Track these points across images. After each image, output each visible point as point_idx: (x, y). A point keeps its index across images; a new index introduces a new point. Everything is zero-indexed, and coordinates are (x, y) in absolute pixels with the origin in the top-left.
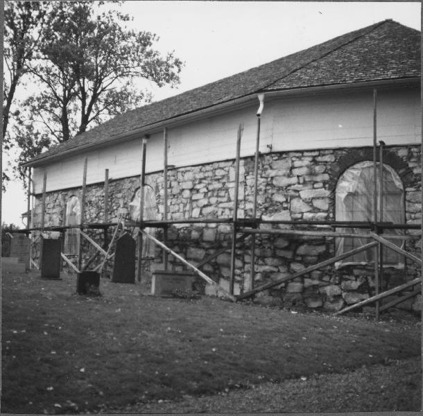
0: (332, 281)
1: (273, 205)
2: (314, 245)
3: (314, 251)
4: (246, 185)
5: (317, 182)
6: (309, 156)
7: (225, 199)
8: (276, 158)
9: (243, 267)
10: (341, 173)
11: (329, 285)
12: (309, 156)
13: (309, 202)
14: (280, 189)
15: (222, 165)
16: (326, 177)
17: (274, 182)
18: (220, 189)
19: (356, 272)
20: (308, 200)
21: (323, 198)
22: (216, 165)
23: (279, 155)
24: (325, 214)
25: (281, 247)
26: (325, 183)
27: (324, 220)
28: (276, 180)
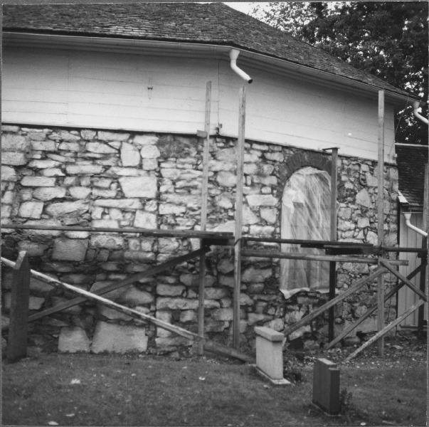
0: (276, 314)
1: (217, 212)
2: (262, 269)
3: (260, 277)
4: (160, 176)
5: (264, 186)
6: (258, 150)
7: (113, 194)
8: (222, 145)
9: (154, 303)
10: (288, 177)
11: (273, 319)
12: (258, 150)
13: (257, 212)
14: (225, 189)
15: (101, 136)
16: (274, 180)
17: (219, 179)
18: (99, 176)
19: (300, 300)
20: (255, 209)
21: (270, 207)
22: (91, 135)
23: (224, 141)
24: (271, 229)
25: (225, 272)
26: (273, 188)
27: (270, 236)
28: (222, 177)
